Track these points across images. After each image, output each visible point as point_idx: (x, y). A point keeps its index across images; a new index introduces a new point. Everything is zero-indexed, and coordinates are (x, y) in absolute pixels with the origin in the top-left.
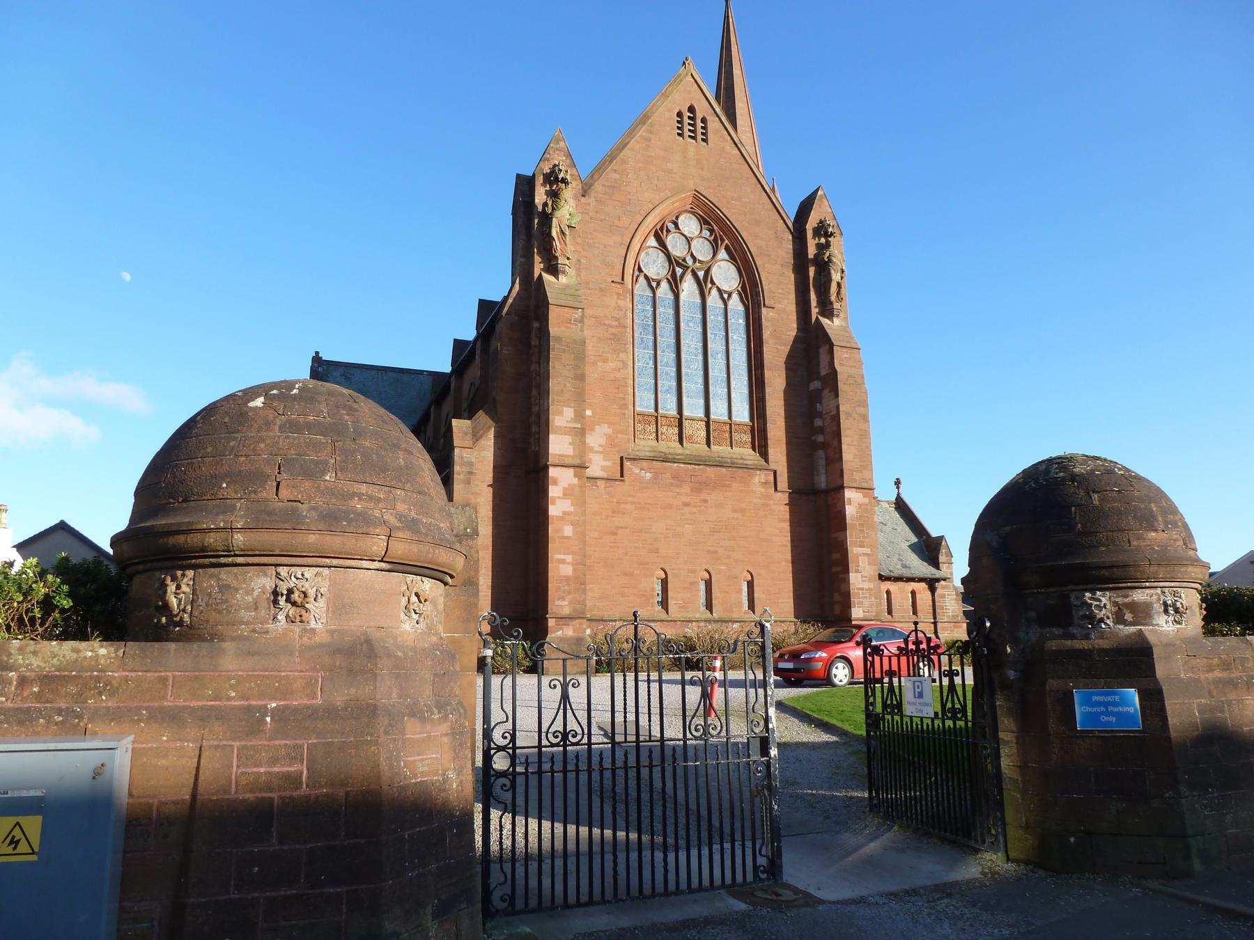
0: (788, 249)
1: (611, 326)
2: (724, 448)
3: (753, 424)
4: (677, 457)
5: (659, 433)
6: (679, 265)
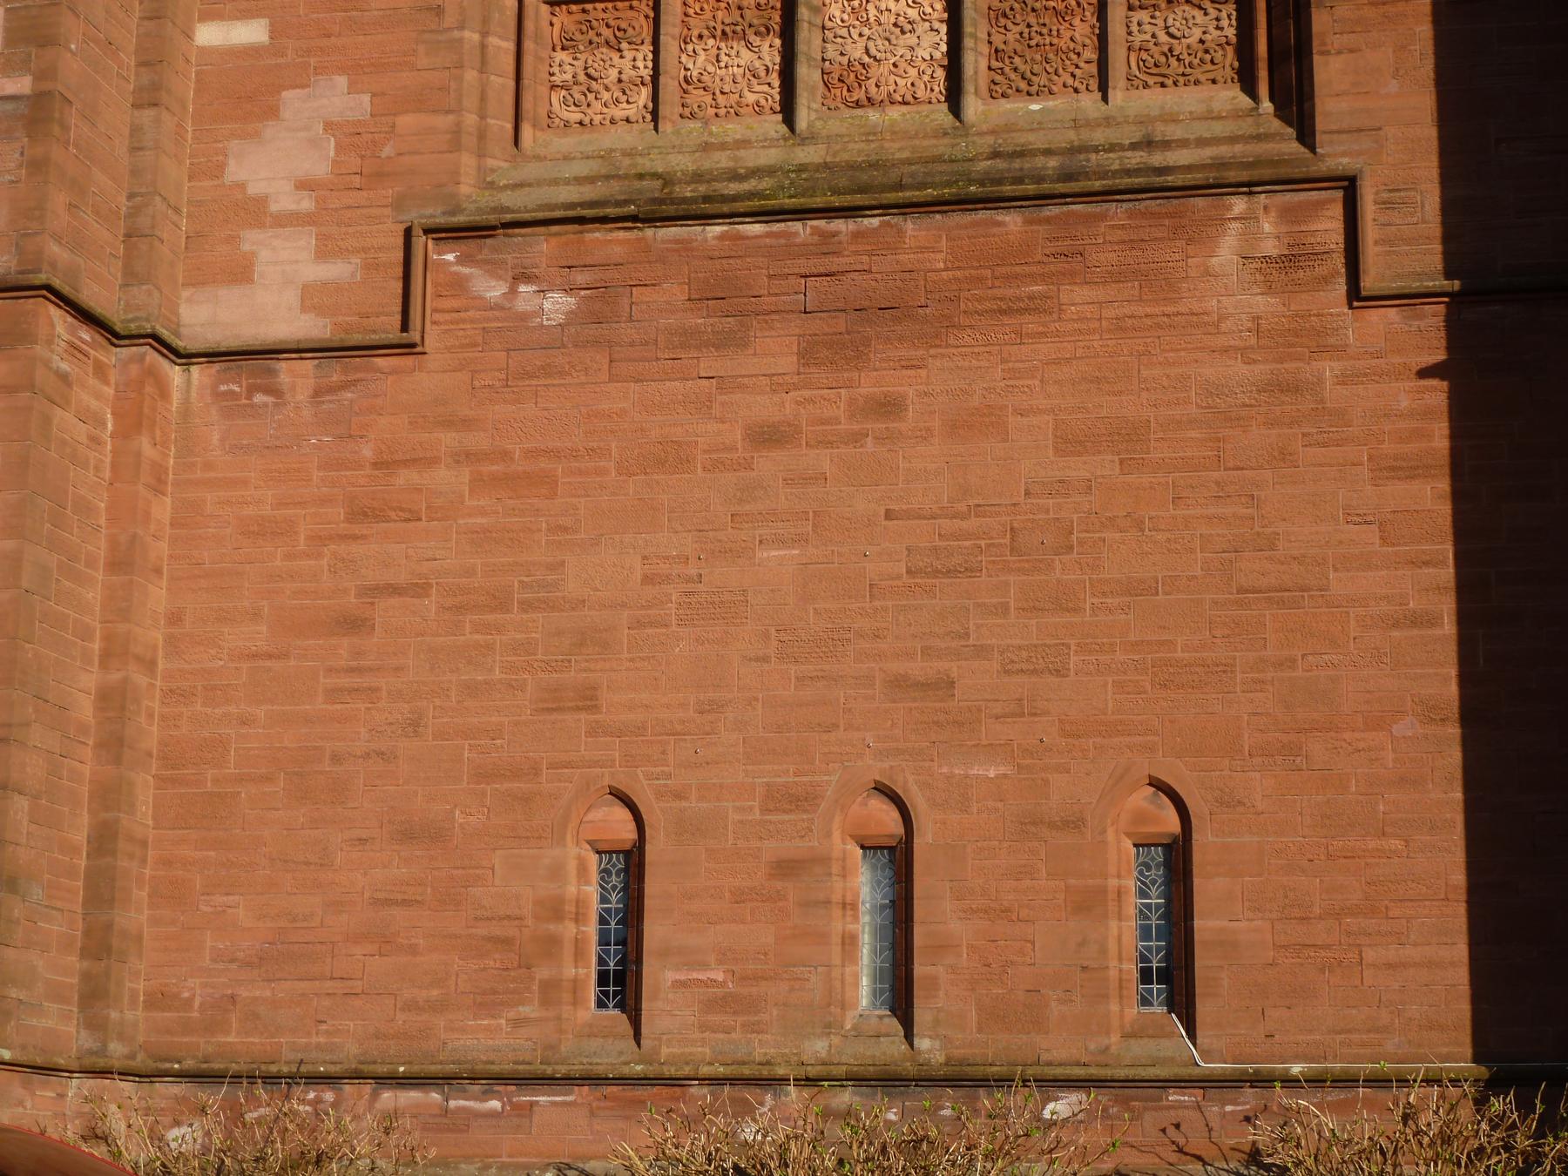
4: (734, 188)
5: (669, 85)
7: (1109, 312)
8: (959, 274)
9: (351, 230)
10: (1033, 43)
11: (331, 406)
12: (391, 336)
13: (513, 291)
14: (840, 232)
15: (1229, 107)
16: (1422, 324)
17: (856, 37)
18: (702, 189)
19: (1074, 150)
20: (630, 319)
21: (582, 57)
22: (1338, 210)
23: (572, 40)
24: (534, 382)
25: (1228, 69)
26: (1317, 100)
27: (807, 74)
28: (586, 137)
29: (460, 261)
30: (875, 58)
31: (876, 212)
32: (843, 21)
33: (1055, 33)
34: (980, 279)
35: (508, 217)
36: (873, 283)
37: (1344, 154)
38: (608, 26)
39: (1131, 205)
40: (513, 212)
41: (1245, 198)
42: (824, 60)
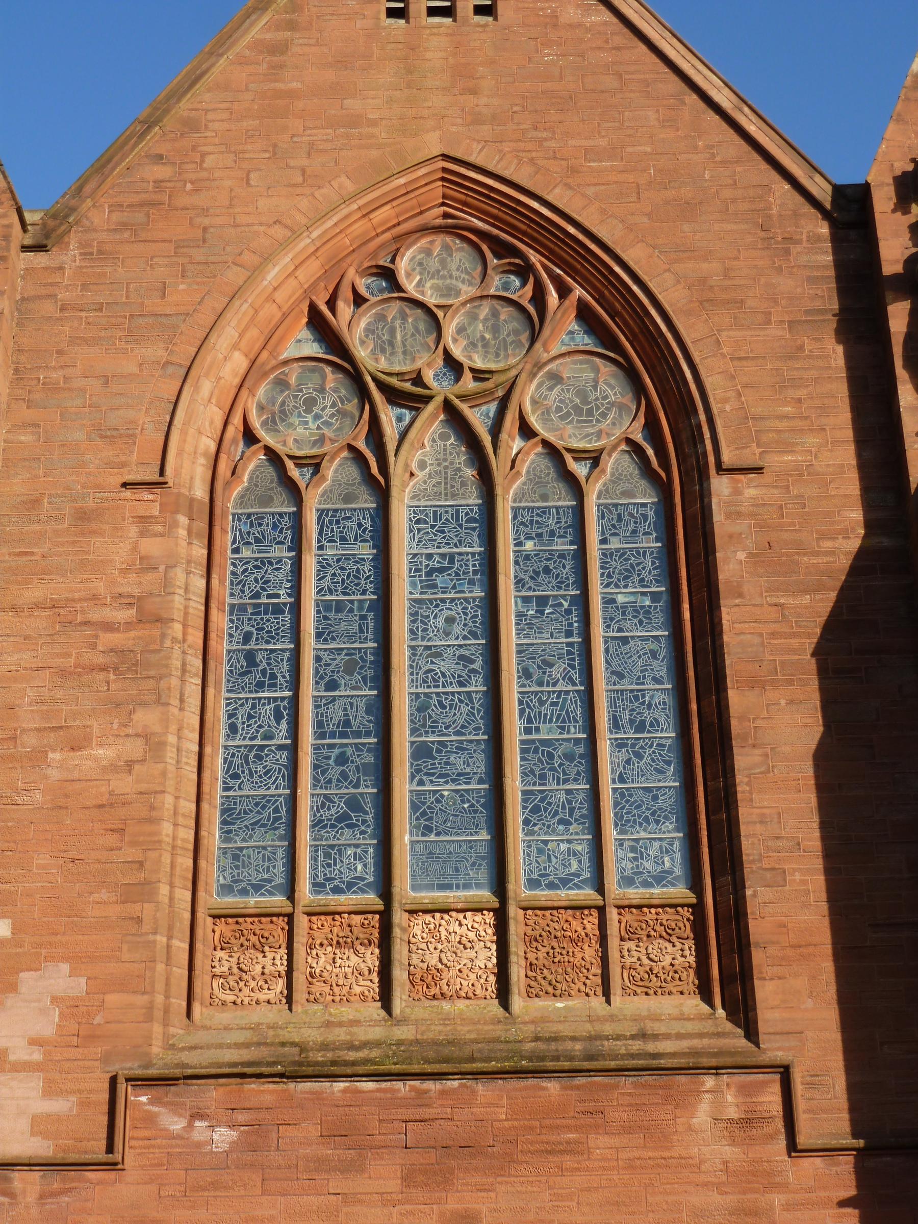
0: (818, 267)
1: (109, 627)
2: (575, 1003)
3: (700, 893)
4: (352, 1055)
5: (300, 979)
6: (394, 396)
7: (624, 1155)
8: (516, 1123)
9: (70, 1076)
10: (556, 960)
11: (53, 1206)
12: (100, 1156)
13: (190, 1125)
14: (431, 1090)
15: (694, 1012)
16: (839, 1169)
17: (432, 949)
18: (330, 1055)
19: (591, 1038)
20: (278, 1149)
21: (236, 955)
22: (776, 1088)
23: (228, 943)
24: (206, 1194)
25: (691, 985)
26: (758, 1011)
27: (399, 975)
28: (239, 1013)
29: (151, 1102)
30: (446, 966)
31: (456, 1077)
32: (423, 938)
33: (571, 954)
34: (532, 1128)
35: (189, 1072)
36: (455, 1128)
37: (779, 1049)
38: (254, 934)
39: (635, 1079)
40: (191, 1068)
41: (714, 1077)
42: (410, 965)
